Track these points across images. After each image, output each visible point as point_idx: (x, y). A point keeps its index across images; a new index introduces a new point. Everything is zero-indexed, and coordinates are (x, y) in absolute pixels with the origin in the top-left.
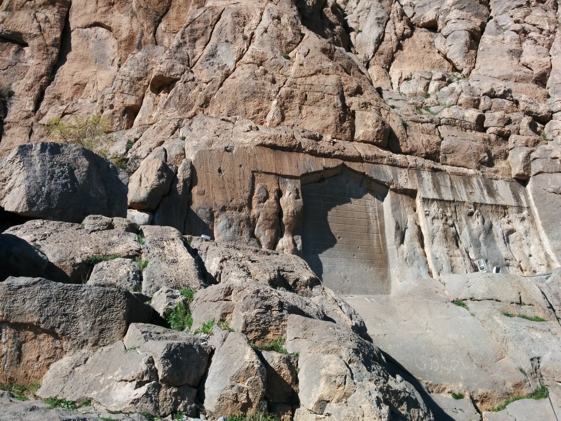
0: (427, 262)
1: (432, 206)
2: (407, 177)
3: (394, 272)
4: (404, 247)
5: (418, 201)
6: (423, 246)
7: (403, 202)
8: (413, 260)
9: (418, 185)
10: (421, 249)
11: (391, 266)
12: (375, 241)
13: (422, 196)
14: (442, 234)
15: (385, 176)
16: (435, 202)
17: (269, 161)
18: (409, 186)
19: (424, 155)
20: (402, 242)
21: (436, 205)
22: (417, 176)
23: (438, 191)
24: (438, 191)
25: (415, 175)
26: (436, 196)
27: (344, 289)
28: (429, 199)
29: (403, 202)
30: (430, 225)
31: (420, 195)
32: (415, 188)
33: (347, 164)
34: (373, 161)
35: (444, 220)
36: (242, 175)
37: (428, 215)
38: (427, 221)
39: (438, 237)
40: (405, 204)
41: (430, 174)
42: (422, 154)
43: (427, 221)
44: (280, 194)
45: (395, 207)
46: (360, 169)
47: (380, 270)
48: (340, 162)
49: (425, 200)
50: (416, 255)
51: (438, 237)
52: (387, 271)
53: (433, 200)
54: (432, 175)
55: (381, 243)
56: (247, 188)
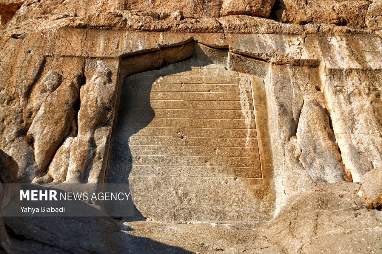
0: (341, 160)
1: (349, 79)
2: (302, 46)
3: (280, 182)
4: (298, 141)
5: (323, 76)
6: (332, 136)
7: (296, 79)
8: (313, 159)
9: (321, 54)
10: (329, 142)
11: (276, 174)
12: (248, 139)
13: (328, 66)
14: (370, 117)
15: (262, 47)
16: (355, 74)
17: (76, 44)
18: (305, 56)
19: (335, 21)
20: (293, 132)
21: (356, 78)
22: (320, 44)
23: (361, 59)
24: (361, 59)
25: (316, 44)
26: (355, 65)
27: (181, 212)
28: (341, 70)
29: (296, 79)
30: (344, 104)
31: (325, 65)
32: (315, 58)
33: (198, 37)
34: (242, 31)
35: (372, 96)
36: (26, 62)
37: (341, 91)
38: (338, 99)
39: (361, 121)
40: (300, 82)
41: (344, 39)
42: (331, 20)
43: (338, 99)
44: (82, 80)
45: (282, 85)
46: (220, 42)
47: (256, 182)
48: (188, 36)
49: (334, 73)
50: (318, 151)
51: (361, 121)
52: (268, 183)
53: (350, 71)
54: (347, 40)
55: (260, 142)
56: (32, 73)
